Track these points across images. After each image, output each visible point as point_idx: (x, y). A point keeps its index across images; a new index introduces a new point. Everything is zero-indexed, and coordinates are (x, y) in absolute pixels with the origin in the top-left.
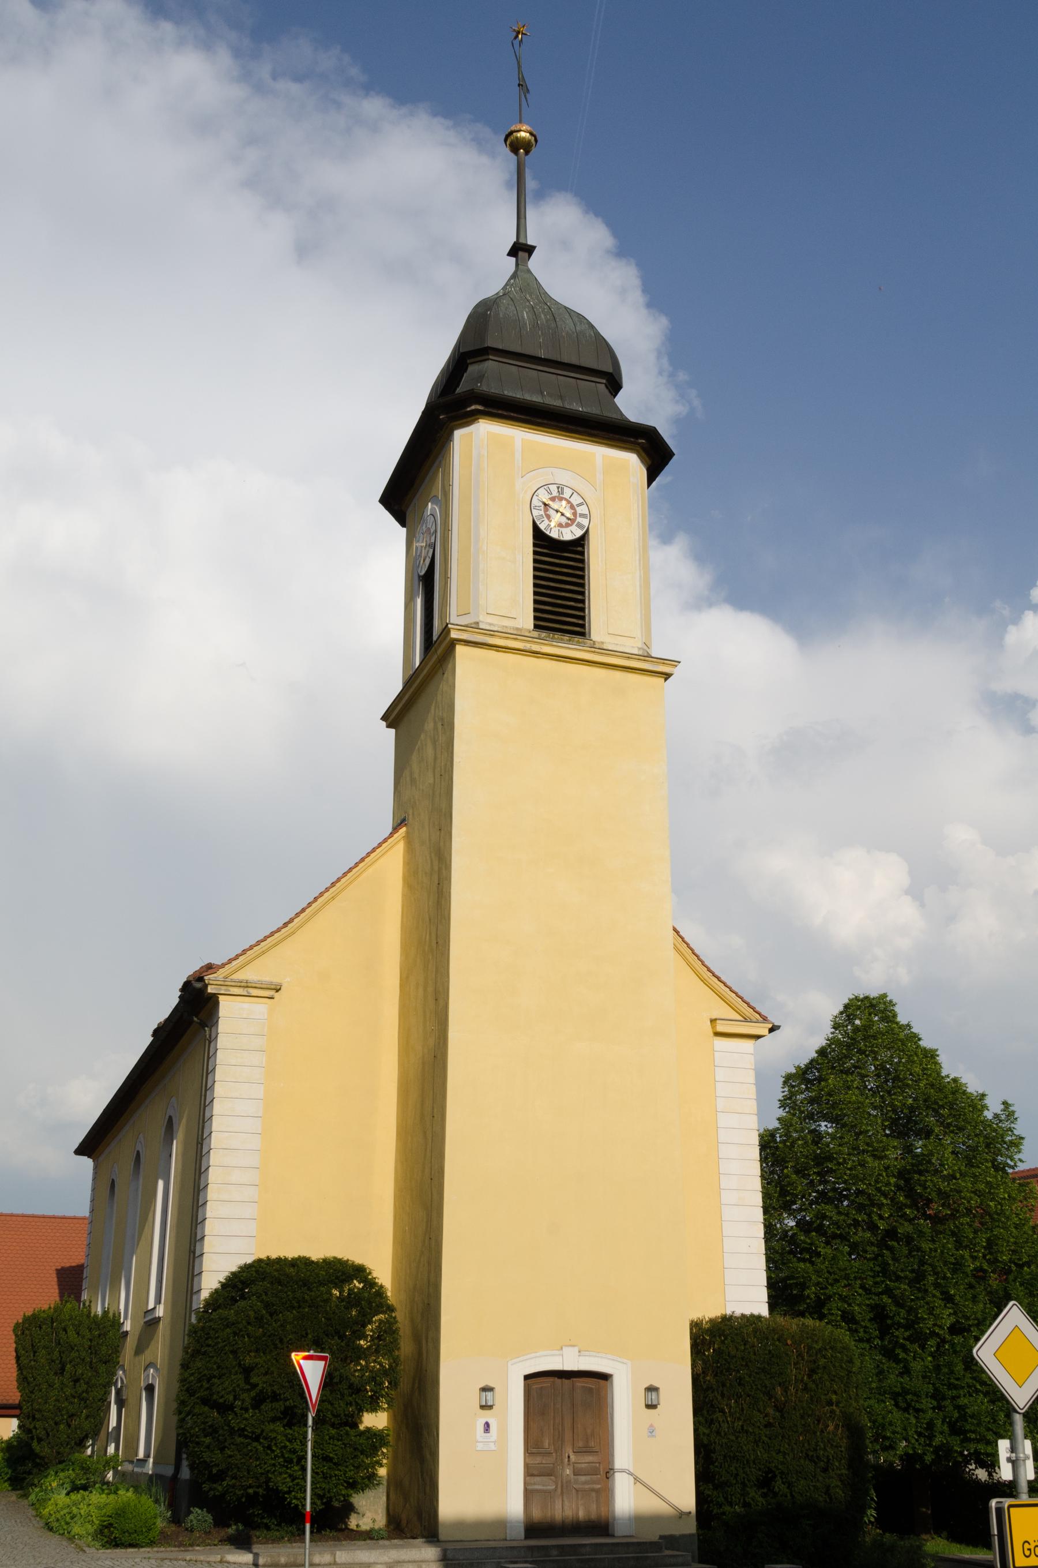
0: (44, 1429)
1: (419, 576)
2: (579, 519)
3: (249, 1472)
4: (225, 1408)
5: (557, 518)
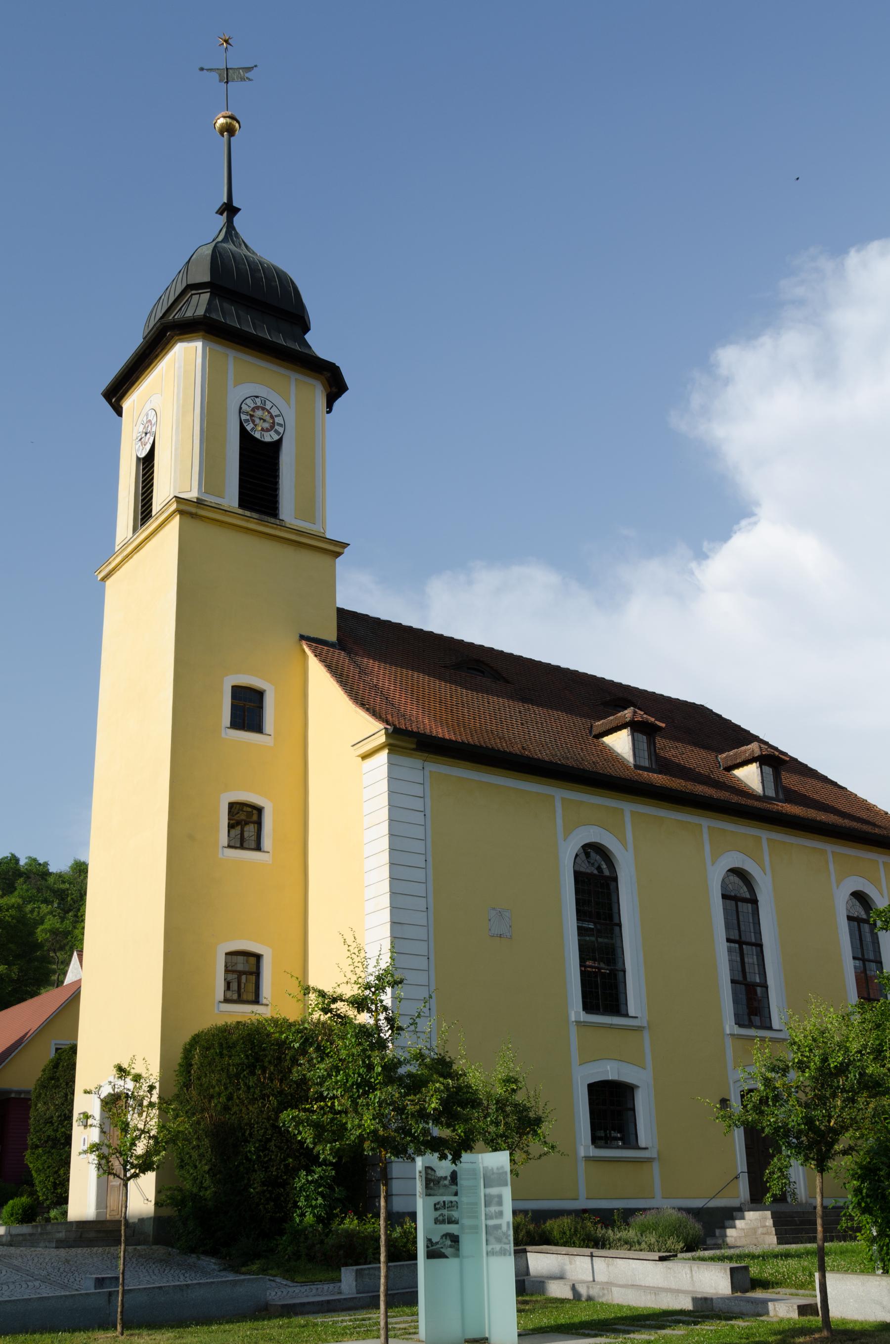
1: (138, 459)
2: (277, 427)
5: (261, 425)
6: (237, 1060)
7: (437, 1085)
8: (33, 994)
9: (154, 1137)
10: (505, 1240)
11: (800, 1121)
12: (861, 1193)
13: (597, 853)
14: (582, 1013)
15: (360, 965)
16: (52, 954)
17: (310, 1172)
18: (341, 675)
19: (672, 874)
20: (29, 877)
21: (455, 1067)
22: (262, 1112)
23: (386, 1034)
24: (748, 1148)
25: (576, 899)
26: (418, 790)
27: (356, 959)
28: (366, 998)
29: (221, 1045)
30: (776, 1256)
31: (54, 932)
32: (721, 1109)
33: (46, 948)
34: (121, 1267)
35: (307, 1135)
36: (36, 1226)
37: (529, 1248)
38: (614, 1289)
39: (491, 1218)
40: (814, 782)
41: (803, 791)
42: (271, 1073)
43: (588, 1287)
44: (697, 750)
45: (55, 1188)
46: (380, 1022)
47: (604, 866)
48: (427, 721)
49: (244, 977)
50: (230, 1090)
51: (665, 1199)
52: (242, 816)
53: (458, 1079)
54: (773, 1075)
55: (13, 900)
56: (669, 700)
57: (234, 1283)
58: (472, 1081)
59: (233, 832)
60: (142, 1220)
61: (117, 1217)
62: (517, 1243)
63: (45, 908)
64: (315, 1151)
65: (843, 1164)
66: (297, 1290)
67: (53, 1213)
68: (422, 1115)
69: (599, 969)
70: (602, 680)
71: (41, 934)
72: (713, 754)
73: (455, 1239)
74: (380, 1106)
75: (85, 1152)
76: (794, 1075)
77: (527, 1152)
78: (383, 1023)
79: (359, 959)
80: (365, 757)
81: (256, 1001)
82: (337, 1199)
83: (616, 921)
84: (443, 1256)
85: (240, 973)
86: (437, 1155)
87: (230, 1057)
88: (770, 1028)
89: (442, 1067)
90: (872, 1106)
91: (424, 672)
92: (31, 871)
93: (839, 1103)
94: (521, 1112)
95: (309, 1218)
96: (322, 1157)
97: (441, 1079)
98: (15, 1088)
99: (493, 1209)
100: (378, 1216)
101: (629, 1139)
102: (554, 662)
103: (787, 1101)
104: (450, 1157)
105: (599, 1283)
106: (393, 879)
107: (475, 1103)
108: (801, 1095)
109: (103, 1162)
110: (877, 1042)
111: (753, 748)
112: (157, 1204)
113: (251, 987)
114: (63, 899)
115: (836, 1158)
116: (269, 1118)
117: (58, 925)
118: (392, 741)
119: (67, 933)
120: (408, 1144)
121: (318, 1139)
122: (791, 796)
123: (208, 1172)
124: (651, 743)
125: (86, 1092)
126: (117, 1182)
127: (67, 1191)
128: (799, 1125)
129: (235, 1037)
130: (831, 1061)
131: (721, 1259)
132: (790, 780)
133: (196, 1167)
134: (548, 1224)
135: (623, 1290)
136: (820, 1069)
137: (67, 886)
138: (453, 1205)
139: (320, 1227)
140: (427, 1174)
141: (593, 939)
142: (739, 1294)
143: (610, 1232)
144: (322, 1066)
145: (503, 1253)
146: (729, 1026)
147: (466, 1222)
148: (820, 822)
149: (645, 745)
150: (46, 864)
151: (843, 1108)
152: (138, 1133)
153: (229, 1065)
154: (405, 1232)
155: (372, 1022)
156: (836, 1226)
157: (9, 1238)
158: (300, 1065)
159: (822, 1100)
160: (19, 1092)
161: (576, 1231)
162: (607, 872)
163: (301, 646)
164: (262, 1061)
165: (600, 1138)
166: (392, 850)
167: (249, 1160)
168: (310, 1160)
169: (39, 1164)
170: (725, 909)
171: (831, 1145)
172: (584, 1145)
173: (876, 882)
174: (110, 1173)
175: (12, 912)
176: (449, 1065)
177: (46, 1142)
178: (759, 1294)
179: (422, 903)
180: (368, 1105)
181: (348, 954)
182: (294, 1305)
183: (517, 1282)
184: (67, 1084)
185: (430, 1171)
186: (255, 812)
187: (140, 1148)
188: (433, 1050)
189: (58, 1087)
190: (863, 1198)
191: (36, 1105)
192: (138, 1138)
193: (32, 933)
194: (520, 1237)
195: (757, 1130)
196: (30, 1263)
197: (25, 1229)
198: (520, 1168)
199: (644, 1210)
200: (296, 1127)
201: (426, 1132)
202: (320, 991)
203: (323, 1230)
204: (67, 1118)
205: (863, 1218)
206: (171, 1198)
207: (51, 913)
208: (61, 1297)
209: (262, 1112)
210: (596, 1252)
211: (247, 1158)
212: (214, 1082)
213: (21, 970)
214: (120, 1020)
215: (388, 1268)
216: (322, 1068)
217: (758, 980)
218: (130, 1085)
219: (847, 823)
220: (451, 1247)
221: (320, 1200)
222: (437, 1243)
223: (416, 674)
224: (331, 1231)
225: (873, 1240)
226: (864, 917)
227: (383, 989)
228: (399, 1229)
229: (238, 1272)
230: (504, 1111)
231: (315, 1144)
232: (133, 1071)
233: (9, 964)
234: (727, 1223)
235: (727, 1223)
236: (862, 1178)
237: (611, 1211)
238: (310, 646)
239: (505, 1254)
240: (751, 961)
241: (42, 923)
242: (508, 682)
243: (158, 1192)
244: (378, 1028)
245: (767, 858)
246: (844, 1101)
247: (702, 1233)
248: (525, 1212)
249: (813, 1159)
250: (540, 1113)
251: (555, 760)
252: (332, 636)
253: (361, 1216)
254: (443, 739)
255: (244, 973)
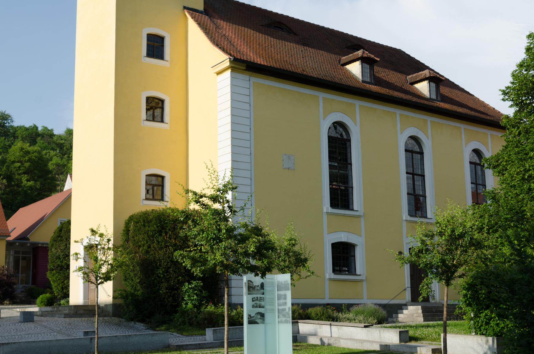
6: (152, 229)
7: (254, 239)
8: (48, 196)
9: (111, 264)
10: (287, 316)
11: (438, 261)
12: (467, 297)
13: (340, 127)
14: (330, 208)
15: (215, 179)
16: (57, 176)
17: (190, 283)
18: (206, 29)
19: (380, 137)
20: (43, 137)
21: (263, 231)
22: (166, 254)
23: (228, 214)
24: (411, 276)
25: (329, 151)
26: (247, 92)
27: (213, 176)
28: (218, 196)
29: (144, 221)
30: (422, 327)
31: (58, 165)
32: (399, 255)
33: (54, 173)
34: (96, 326)
35: (187, 263)
36: (54, 308)
37: (299, 321)
38: (341, 340)
39: (281, 305)
40: (457, 92)
41: (451, 96)
42: (170, 235)
43: (329, 339)
44: (395, 73)
45: (63, 290)
46: (225, 208)
47: (344, 133)
48: (252, 55)
49: (155, 188)
50: (149, 243)
51: (369, 299)
52: (153, 104)
53: (265, 237)
54: (426, 238)
55: (36, 148)
56: (382, 46)
57: (153, 335)
58: (272, 239)
59: (149, 113)
60: (106, 305)
61: (94, 304)
62: (293, 318)
63: (52, 153)
64: (192, 271)
65: (459, 282)
66: (184, 339)
67: (62, 302)
68: (246, 254)
69: (339, 186)
70: (347, 35)
71: (51, 166)
72: (405, 76)
73: (262, 315)
74: (225, 249)
75: (76, 271)
76: (437, 239)
77: (299, 275)
78: (226, 209)
79: (214, 176)
80: (218, 73)
81: (162, 199)
82: (204, 297)
83: (349, 162)
84: (256, 323)
85: (154, 186)
86: (253, 274)
87: (149, 227)
88: (426, 217)
89: (257, 231)
90: (475, 254)
91: (250, 28)
92: (44, 133)
93: (459, 252)
94: (297, 256)
95: (190, 305)
96: (195, 274)
97: (256, 237)
98: (41, 242)
99: (282, 301)
100: (223, 305)
101: (351, 270)
102: (321, 24)
103: (432, 252)
104: (260, 275)
105: (334, 338)
106: (233, 138)
107: (273, 249)
108: (440, 249)
109: (86, 276)
110: (481, 224)
111: (426, 73)
112: (113, 298)
113: (159, 193)
114: (61, 148)
115: (456, 279)
116: (169, 257)
117: (60, 162)
118: (233, 65)
119: (64, 166)
120: (239, 268)
121: (193, 265)
122: (444, 99)
123: (139, 283)
124: (372, 69)
125: (75, 242)
126: (93, 286)
127: (69, 291)
128: (438, 263)
129: (151, 217)
130: (456, 232)
131: (395, 327)
132: (445, 90)
133: (133, 280)
134: (309, 310)
135: (345, 341)
136: (450, 236)
137: (63, 141)
138: (261, 299)
139: (195, 310)
140: (249, 284)
141: (337, 171)
142: (403, 343)
143: (340, 314)
144: (195, 229)
145: (286, 322)
146: (405, 216)
147: (268, 307)
148: (459, 112)
149: (368, 70)
150: (52, 130)
151: (461, 255)
152: (103, 262)
153: (148, 231)
154: (238, 313)
155: (221, 208)
156: (454, 314)
157: (41, 313)
158: (184, 229)
159: (450, 251)
160: (43, 244)
161: (323, 313)
162: (345, 137)
163: (184, 12)
164: (166, 229)
165: (337, 270)
166: (232, 123)
167: (159, 277)
168: (190, 277)
169: (54, 278)
170: (406, 157)
171: (453, 273)
172: (329, 273)
173: (486, 145)
174: (89, 281)
175: (36, 154)
176: (261, 230)
177: (57, 267)
178: (413, 343)
179: (248, 151)
180: (218, 249)
181: (209, 173)
182: (183, 345)
183: (293, 336)
184: (67, 239)
185: (250, 283)
186: (160, 102)
187: (104, 270)
188: (252, 223)
189: (62, 241)
190: (467, 299)
191: (51, 250)
192: (103, 264)
193: (46, 165)
194: (295, 316)
195: (417, 265)
196: (51, 324)
197: (49, 309)
198: (296, 283)
199: (358, 304)
200: (182, 259)
201: (248, 262)
202: (194, 192)
203: (197, 311)
204: (68, 256)
205: (467, 308)
206: (121, 295)
207: (56, 155)
208: (67, 340)
209: (166, 254)
210: (333, 323)
211: (158, 276)
212: (141, 239)
213: (41, 184)
214: (92, 207)
215: (228, 329)
216: (195, 230)
217: (421, 194)
218: (98, 238)
219: (473, 113)
220: (260, 319)
221: (195, 297)
222: (253, 317)
223: (246, 29)
224: (200, 311)
225: (472, 319)
226: (478, 162)
227: (227, 192)
228: (235, 311)
229: (154, 330)
230: (288, 255)
231: (192, 267)
232: (99, 232)
233: (35, 181)
234: (399, 311)
235: (399, 311)
236: (468, 289)
237: (341, 305)
238: (189, 13)
239: (287, 323)
240: (418, 183)
241: (51, 160)
242: (296, 35)
243: (114, 291)
244: (224, 211)
245: (429, 131)
246: (461, 252)
247: (386, 315)
248: (298, 304)
249: (444, 279)
250: (307, 256)
251: (320, 77)
252: (201, 7)
253: (216, 305)
254: (260, 65)
255: (156, 185)
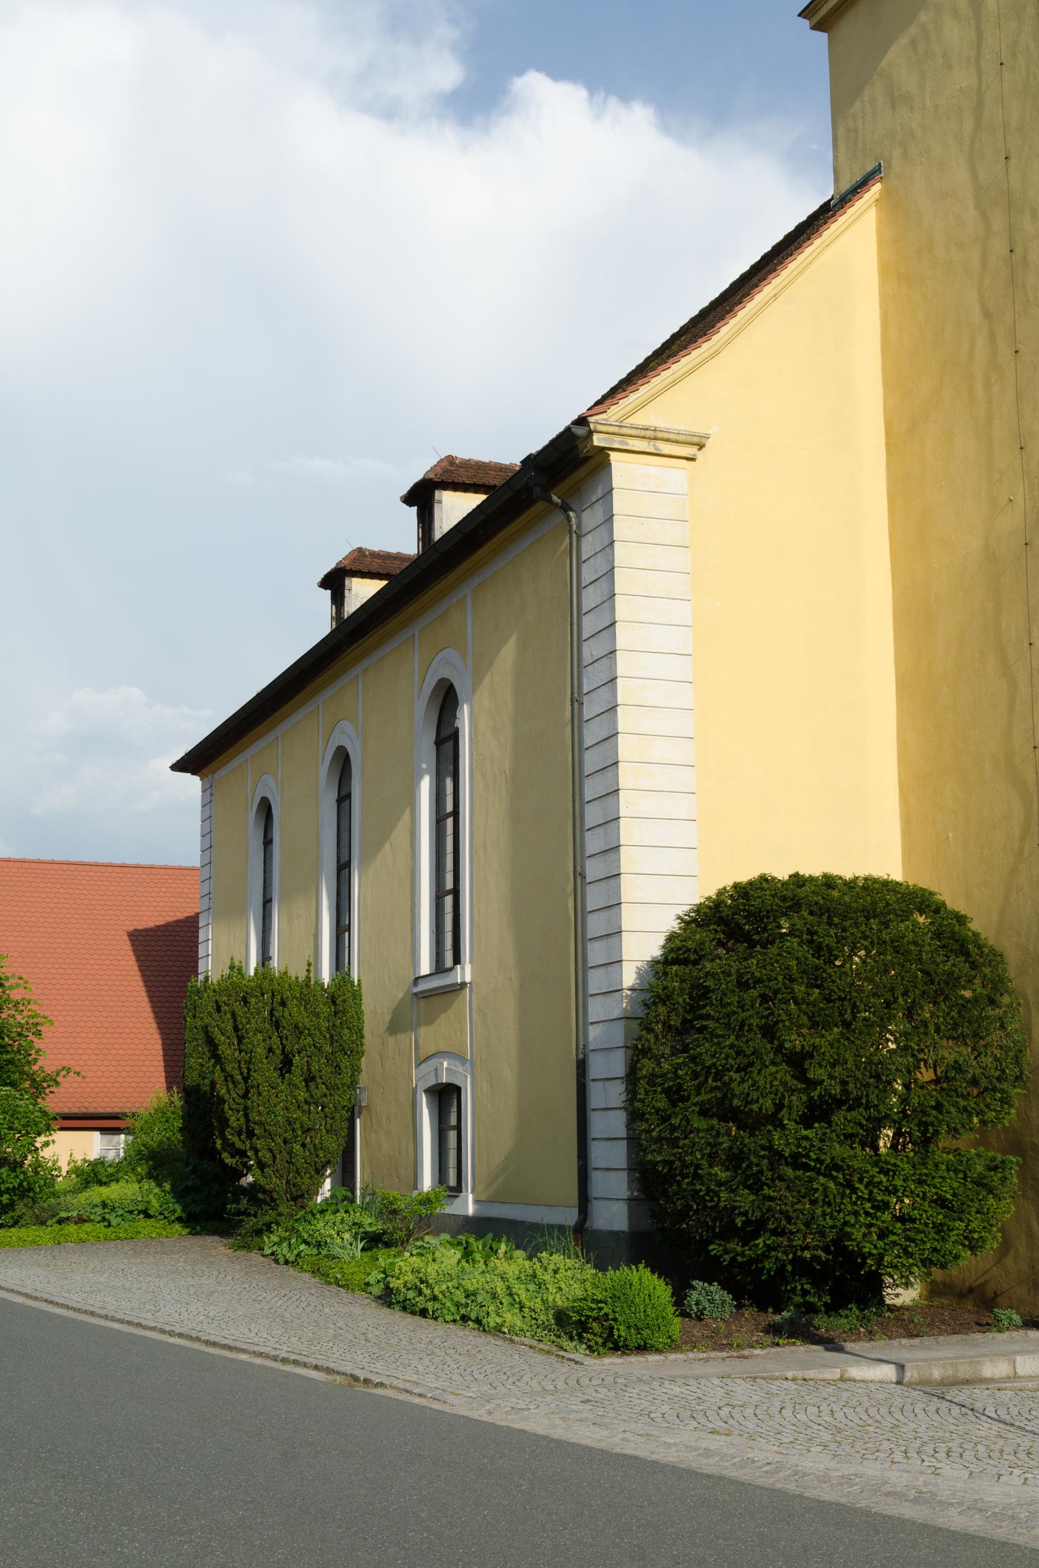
0: (271, 1151)
3: (807, 1225)
4: (751, 1122)
